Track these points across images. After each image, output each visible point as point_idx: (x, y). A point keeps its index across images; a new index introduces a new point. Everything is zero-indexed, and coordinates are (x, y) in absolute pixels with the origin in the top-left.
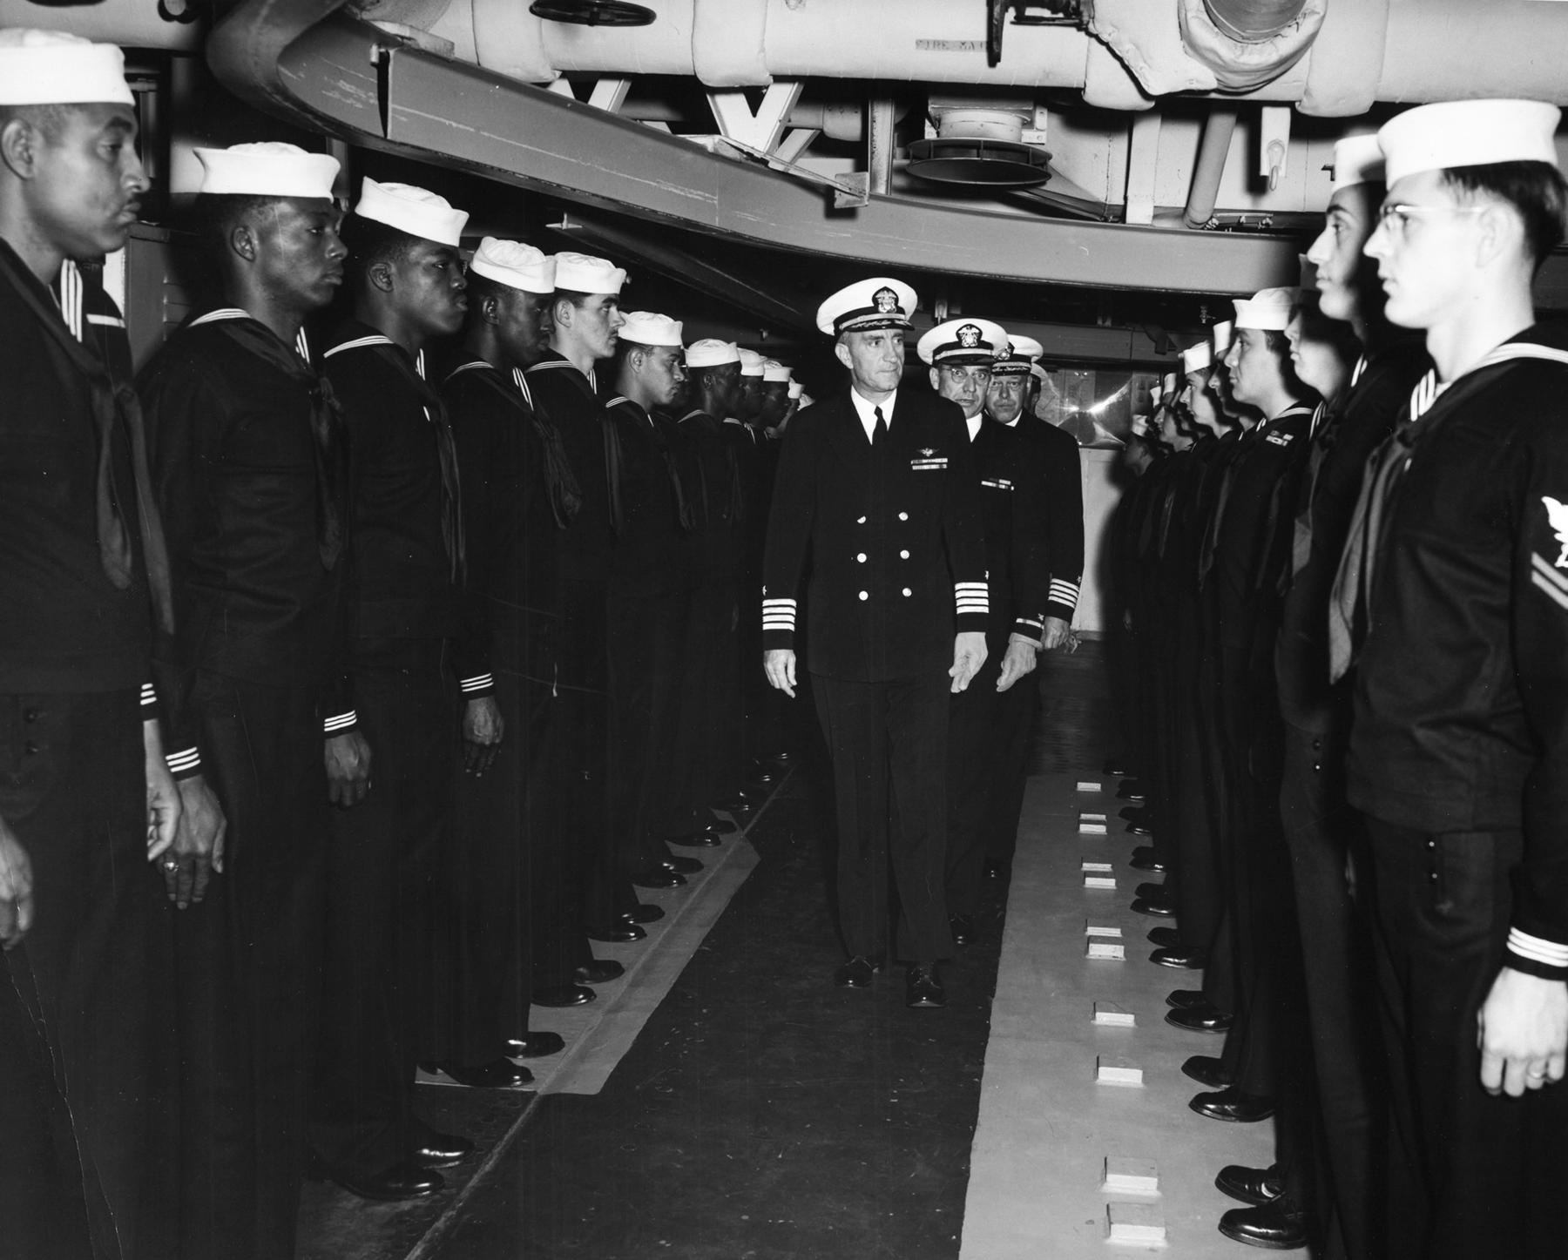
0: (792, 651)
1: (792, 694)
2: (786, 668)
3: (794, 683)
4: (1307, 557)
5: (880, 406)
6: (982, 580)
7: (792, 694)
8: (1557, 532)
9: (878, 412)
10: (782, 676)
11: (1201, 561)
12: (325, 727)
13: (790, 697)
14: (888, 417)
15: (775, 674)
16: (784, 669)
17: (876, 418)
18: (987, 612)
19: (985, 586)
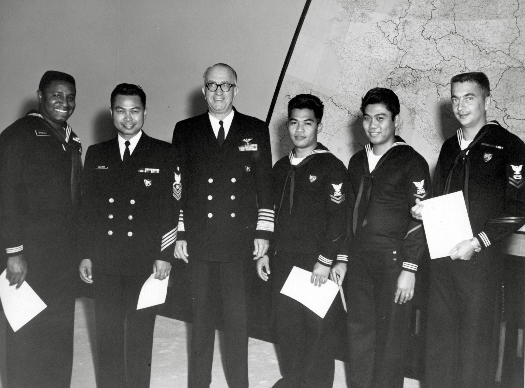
0: (268, 241)
1: (187, 261)
2: (182, 248)
3: (187, 255)
4: (415, 196)
5: (223, 121)
6: (272, 209)
7: (187, 261)
8: (418, 188)
9: (221, 123)
10: (181, 252)
11: (445, 192)
12: (332, 262)
13: (185, 262)
14: (132, 148)
15: (178, 252)
16: (181, 249)
17: (219, 126)
18: (272, 230)
19: (273, 212)
